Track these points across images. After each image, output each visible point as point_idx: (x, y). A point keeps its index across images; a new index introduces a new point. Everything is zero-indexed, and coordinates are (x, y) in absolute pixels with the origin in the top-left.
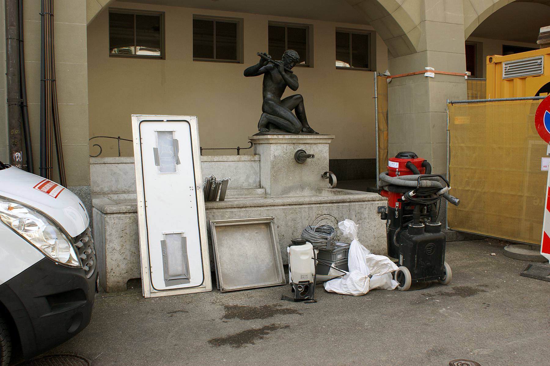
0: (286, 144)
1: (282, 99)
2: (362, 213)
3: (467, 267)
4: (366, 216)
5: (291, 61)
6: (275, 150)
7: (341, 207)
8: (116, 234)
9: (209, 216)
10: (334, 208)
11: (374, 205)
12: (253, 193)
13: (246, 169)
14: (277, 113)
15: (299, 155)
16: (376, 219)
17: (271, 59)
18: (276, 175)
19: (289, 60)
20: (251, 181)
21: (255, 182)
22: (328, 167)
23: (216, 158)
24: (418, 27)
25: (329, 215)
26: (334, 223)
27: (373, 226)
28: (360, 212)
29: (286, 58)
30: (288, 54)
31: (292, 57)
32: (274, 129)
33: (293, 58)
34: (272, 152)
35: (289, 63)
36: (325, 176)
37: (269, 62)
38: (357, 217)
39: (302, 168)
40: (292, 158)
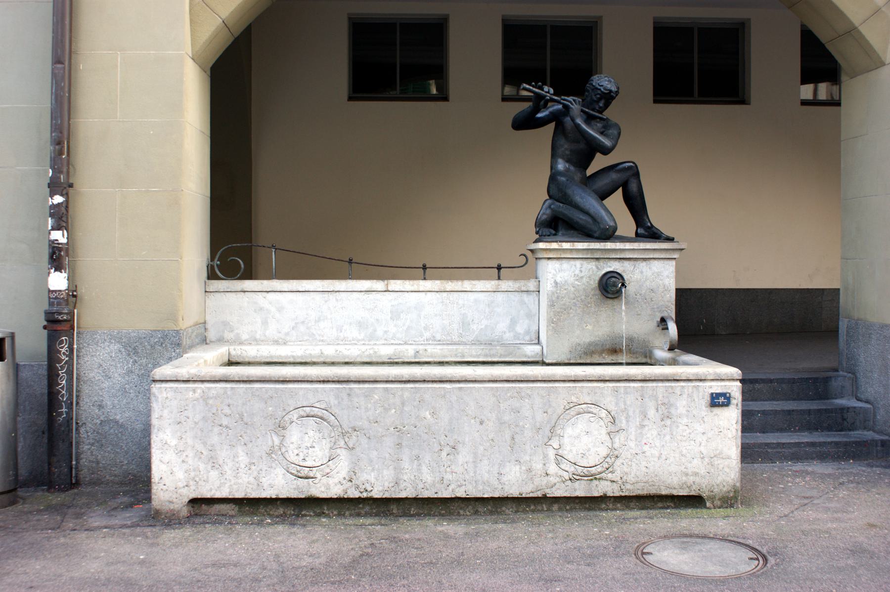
1: (590, 172)
2: (671, 405)
4: (682, 410)
5: (598, 96)
6: (557, 270)
7: (622, 390)
8: (168, 417)
9: (341, 394)
10: (606, 392)
11: (701, 389)
13: (511, 307)
16: (706, 419)
17: (551, 94)
18: (558, 319)
19: (595, 95)
20: (520, 329)
21: (528, 332)
22: (673, 307)
23: (450, 285)
24: (883, 9)
25: (593, 406)
26: (606, 421)
27: (697, 434)
28: (666, 403)
30: (594, 84)
31: (600, 89)
33: (601, 91)
34: (550, 276)
35: (595, 101)
38: (660, 411)
39: (615, 307)
40: (594, 286)
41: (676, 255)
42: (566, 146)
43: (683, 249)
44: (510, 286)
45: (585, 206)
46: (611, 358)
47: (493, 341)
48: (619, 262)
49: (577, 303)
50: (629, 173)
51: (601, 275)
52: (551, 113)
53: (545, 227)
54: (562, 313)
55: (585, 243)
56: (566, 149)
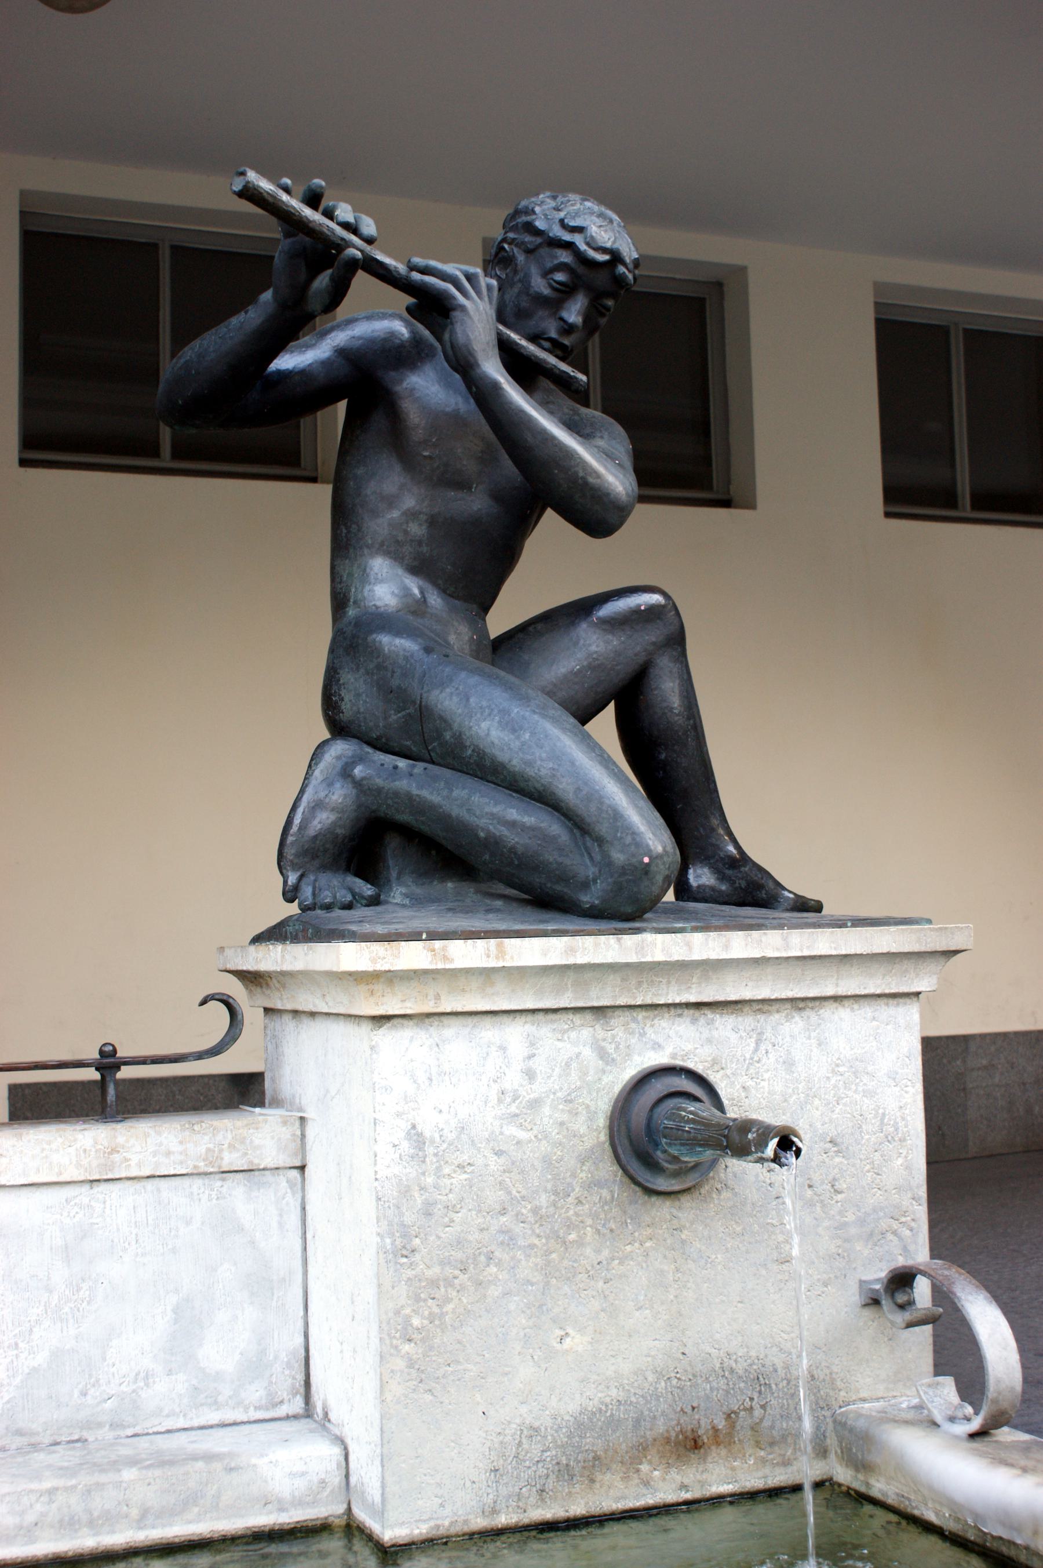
0: (521, 1020)
3: (177, 363)
5: (560, 277)
12: (218, 1496)
13: (174, 1251)
14: (448, 736)
15: (650, 1119)
19: (546, 273)
29: (521, 258)
30: (540, 224)
31: (569, 246)
32: (424, 874)
36: (901, 1298)
37: (353, 266)
40: (589, 1143)
41: (924, 982)
42: (409, 502)
43: (956, 952)
44: (168, 1153)
45: (529, 764)
46: (676, 1476)
47: (90, 1425)
48: (694, 1021)
49: (518, 1229)
50: (652, 635)
51: (617, 1089)
52: (342, 352)
53: (324, 868)
54: (449, 1283)
55: (554, 941)
56: (411, 515)
